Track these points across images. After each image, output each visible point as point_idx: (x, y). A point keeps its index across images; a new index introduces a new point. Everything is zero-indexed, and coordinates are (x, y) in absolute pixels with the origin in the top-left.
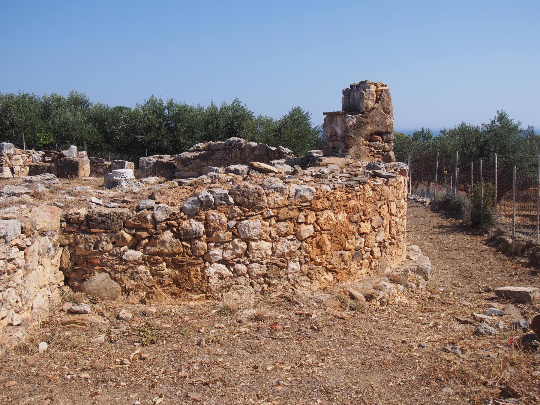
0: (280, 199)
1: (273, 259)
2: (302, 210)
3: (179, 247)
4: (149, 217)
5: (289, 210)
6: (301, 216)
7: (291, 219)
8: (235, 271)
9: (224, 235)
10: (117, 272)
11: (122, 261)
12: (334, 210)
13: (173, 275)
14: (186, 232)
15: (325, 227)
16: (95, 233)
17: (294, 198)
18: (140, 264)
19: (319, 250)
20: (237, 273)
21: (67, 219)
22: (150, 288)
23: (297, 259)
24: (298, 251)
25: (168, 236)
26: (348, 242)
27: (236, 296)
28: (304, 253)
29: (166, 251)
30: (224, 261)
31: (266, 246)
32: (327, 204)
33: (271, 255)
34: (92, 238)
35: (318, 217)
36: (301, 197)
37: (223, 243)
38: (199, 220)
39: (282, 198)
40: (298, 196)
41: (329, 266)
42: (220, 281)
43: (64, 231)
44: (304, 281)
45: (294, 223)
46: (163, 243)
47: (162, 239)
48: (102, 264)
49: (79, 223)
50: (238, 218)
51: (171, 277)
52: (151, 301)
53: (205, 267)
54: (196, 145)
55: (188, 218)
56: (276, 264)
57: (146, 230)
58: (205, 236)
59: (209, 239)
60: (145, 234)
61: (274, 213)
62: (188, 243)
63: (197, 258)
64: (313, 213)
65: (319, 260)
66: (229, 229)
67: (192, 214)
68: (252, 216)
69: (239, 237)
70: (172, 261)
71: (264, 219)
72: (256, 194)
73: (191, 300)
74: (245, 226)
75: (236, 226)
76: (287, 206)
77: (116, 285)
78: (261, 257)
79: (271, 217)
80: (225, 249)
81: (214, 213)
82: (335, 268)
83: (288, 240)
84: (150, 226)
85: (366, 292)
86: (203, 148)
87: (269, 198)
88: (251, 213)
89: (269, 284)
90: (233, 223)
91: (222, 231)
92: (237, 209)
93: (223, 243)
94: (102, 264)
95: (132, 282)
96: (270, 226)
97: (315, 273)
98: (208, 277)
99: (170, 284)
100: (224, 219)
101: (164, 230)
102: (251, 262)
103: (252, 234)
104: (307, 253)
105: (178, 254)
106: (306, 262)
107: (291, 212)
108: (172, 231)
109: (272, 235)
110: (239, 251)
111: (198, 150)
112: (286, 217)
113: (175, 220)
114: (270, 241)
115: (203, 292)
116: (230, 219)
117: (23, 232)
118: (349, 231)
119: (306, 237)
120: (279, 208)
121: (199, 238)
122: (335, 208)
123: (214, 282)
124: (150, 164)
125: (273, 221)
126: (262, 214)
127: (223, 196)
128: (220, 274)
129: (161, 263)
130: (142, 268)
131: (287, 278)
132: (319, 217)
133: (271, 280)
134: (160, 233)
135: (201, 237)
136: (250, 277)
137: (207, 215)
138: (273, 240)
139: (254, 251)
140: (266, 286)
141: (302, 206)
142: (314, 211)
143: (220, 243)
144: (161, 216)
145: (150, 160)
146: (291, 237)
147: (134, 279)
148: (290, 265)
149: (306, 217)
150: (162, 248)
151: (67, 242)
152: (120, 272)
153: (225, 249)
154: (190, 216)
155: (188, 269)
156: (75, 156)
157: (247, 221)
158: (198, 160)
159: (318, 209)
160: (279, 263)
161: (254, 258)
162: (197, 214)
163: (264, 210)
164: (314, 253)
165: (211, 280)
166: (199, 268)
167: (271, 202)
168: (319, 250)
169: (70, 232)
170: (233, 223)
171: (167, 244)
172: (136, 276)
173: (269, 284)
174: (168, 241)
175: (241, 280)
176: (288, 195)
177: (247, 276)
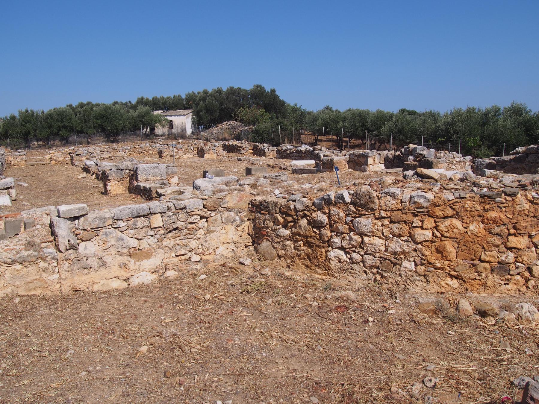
0: (391, 203)
1: (385, 255)
2: (417, 215)
3: (311, 231)
4: (292, 207)
5: (403, 213)
6: (417, 222)
7: (405, 222)
8: (351, 258)
9: (342, 227)
10: (275, 243)
11: (277, 236)
12: (463, 219)
13: (306, 251)
14: (315, 221)
15: (446, 234)
16: (264, 214)
17: (408, 203)
18: (288, 240)
19: (440, 255)
20: (352, 261)
21: (252, 203)
22: (293, 257)
23: (412, 259)
24: (413, 252)
25: (304, 222)
26: (485, 253)
27: (351, 278)
28: (420, 255)
29: (302, 233)
30: (342, 248)
31: (379, 242)
32: (449, 212)
33: (385, 251)
34: (262, 217)
35: (437, 224)
36: (415, 203)
37: (342, 234)
38: (324, 213)
39: (394, 202)
40: (412, 201)
41: (453, 273)
42: (339, 264)
43: (251, 211)
44: (419, 281)
45: (409, 226)
46: (300, 227)
47: (300, 224)
48: (268, 236)
49: (257, 206)
50: (353, 216)
51: (305, 253)
52: (293, 267)
53: (328, 251)
54: (517, 149)
55: (318, 211)
56: (389, 260)
57: (291, 216)
58: (328, 226)
59: (332, 229)
60: (290, 219)
61: (386, 214)
62: (317, 229)
63: (324, 242)
64: (432, 220)
65: (438, 265)
66: (346, 223)
67: (320, 208)
68: (365, 215)
69: (354, 231)
70: (307, 241)
71: (376, 219)
72: (367, 197)
73: (317, 273)
74: (358, 222)
75: (352, 221)
76: (401, 210)
77: (274, 251)
78: (374, 251)
79: (384, 218)
80: (343, 239)
81: (335, 209)
82: (462, 276)
83: (402, 240)
84: (293, 213)
85: (481, 306)
86: (522, 151)
87: (380, 201)
88: (364, 212)
89: (382, 277)
90: (349, 219)
91: (340, 224)
92: (352, 208)
93: (342, 234)
94: (268, 236)
95: (283, 251)
96: (382, 225)
97: (433, 276)
98: (329, 259)
99: (305, 258)
100: (342, 215)
101: (302, 218)
102: (366, 254)
103: (364, 229)
104: (423, 255)
105: (311, 237)
106: (422, 264)
107: (405, 216)
108: (307, 219)
109: (385, 234)
110: (354, 243)
111: (517, 153)
112: (399, 220)
113: (308, 211)
114: (383, 239)
115: (326, 270)
116: (347, 215)
117: (204, 207)
118: (488, 242)
119: (421, 240)
120: (392, 210)
121: (324, 227)
122: (464, 218)
123: (334, 264)
124: (483, 164)
125: (386, 222)
126: (374, 214)
127: (340, 196)
128: (339, 258)
129: (299, 241)
130: (288, 242)
131: (400, 274)
132: (437, 224)
133: (383, 273)
134: (299, 220)
135: (325, 226)
136: (364, 266)
137: (329, 210)
138: (386, 238)
139: (367, 245)
140: (378, 277)
141: (418, 212)
142: (434, 218)
143: (339, 234)
144: (299, 207)
145: (484, 161)
146: (406, 238)
147: (283, 249)
148: (403, 263)
149: (422, 222)
150: (300, 231)
151: (251, 217)
152: (277, 243)
153: (343, 239)
154: (319, 210)
155: (316, 249)
156: (433, 157)
157: (360, 218)
158: (513, 163)
159: (437, 216)
160: (392, 261)
161: (367, 250)
162: (323, 209)
163: (376, 211)
164: (432, 257)
165: (331, 262)
166: (323, 250)
167: (383, 204)
168: (440, 255)
169: (253, 212)
170: (349, 219)
171: (303, 228)
172: (285, 248)
173: (382, 277)
174: (303, 226)
175: (355, 266)
176: (401, 200)
177: (362, 264)
